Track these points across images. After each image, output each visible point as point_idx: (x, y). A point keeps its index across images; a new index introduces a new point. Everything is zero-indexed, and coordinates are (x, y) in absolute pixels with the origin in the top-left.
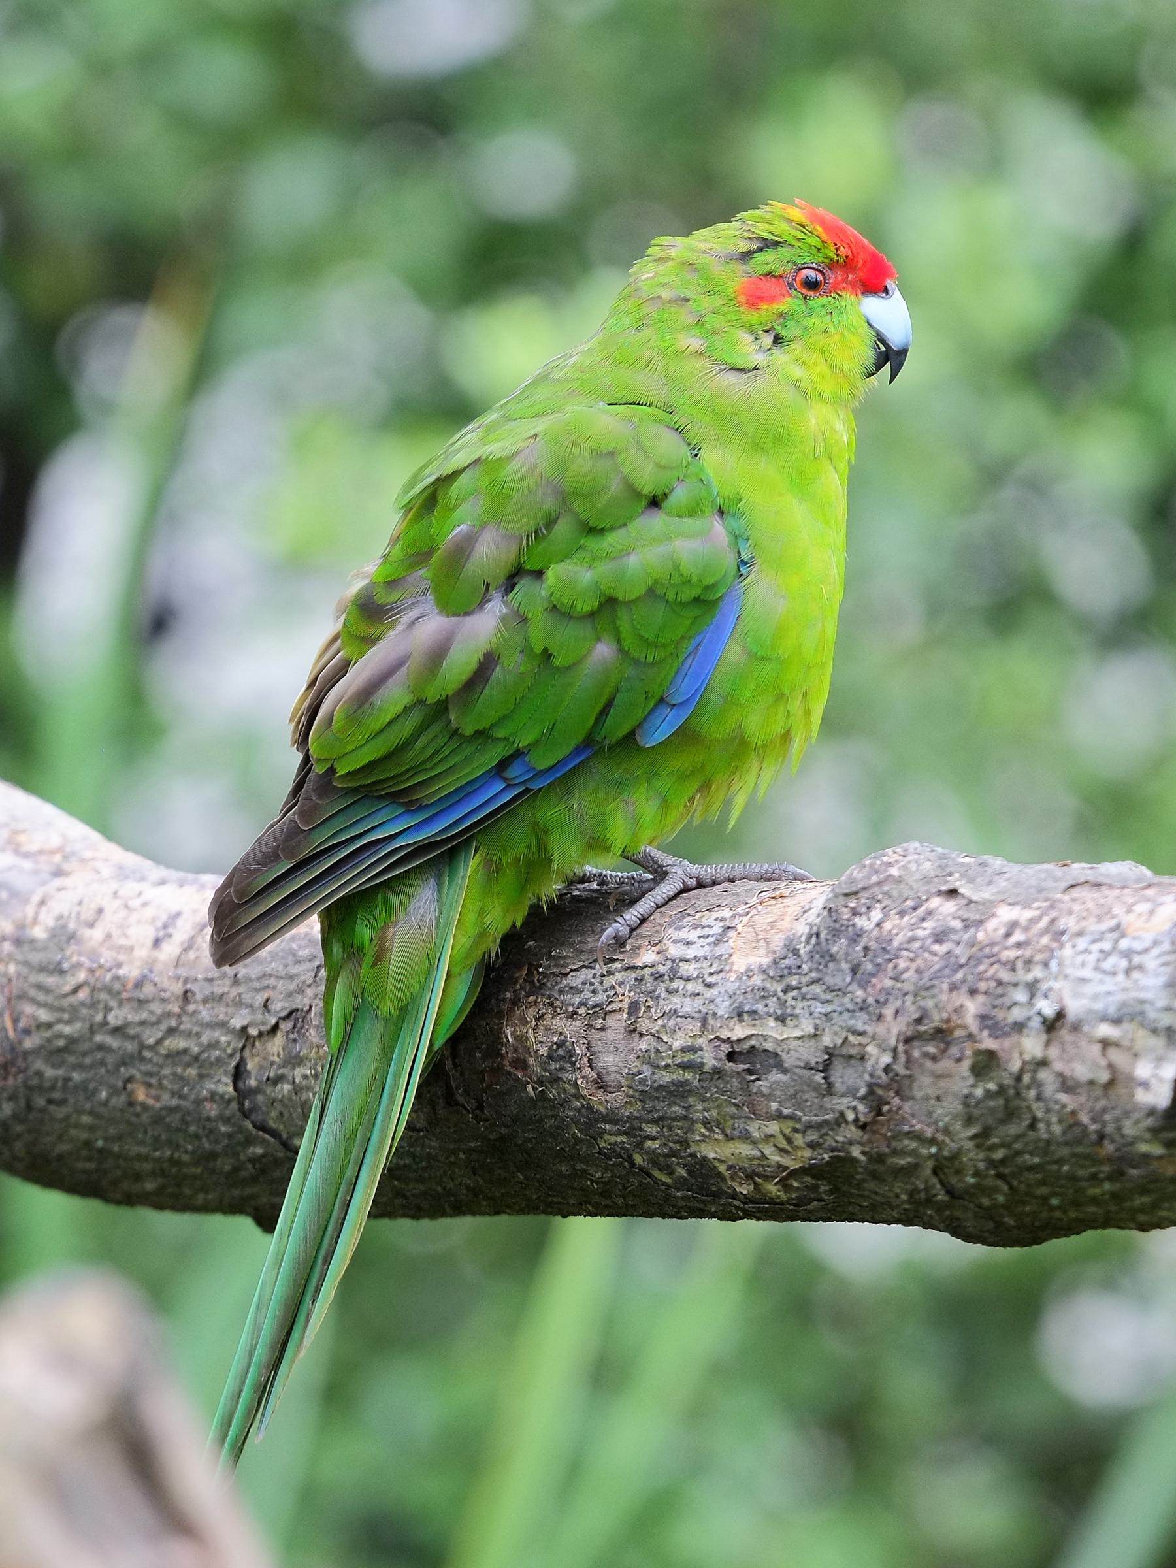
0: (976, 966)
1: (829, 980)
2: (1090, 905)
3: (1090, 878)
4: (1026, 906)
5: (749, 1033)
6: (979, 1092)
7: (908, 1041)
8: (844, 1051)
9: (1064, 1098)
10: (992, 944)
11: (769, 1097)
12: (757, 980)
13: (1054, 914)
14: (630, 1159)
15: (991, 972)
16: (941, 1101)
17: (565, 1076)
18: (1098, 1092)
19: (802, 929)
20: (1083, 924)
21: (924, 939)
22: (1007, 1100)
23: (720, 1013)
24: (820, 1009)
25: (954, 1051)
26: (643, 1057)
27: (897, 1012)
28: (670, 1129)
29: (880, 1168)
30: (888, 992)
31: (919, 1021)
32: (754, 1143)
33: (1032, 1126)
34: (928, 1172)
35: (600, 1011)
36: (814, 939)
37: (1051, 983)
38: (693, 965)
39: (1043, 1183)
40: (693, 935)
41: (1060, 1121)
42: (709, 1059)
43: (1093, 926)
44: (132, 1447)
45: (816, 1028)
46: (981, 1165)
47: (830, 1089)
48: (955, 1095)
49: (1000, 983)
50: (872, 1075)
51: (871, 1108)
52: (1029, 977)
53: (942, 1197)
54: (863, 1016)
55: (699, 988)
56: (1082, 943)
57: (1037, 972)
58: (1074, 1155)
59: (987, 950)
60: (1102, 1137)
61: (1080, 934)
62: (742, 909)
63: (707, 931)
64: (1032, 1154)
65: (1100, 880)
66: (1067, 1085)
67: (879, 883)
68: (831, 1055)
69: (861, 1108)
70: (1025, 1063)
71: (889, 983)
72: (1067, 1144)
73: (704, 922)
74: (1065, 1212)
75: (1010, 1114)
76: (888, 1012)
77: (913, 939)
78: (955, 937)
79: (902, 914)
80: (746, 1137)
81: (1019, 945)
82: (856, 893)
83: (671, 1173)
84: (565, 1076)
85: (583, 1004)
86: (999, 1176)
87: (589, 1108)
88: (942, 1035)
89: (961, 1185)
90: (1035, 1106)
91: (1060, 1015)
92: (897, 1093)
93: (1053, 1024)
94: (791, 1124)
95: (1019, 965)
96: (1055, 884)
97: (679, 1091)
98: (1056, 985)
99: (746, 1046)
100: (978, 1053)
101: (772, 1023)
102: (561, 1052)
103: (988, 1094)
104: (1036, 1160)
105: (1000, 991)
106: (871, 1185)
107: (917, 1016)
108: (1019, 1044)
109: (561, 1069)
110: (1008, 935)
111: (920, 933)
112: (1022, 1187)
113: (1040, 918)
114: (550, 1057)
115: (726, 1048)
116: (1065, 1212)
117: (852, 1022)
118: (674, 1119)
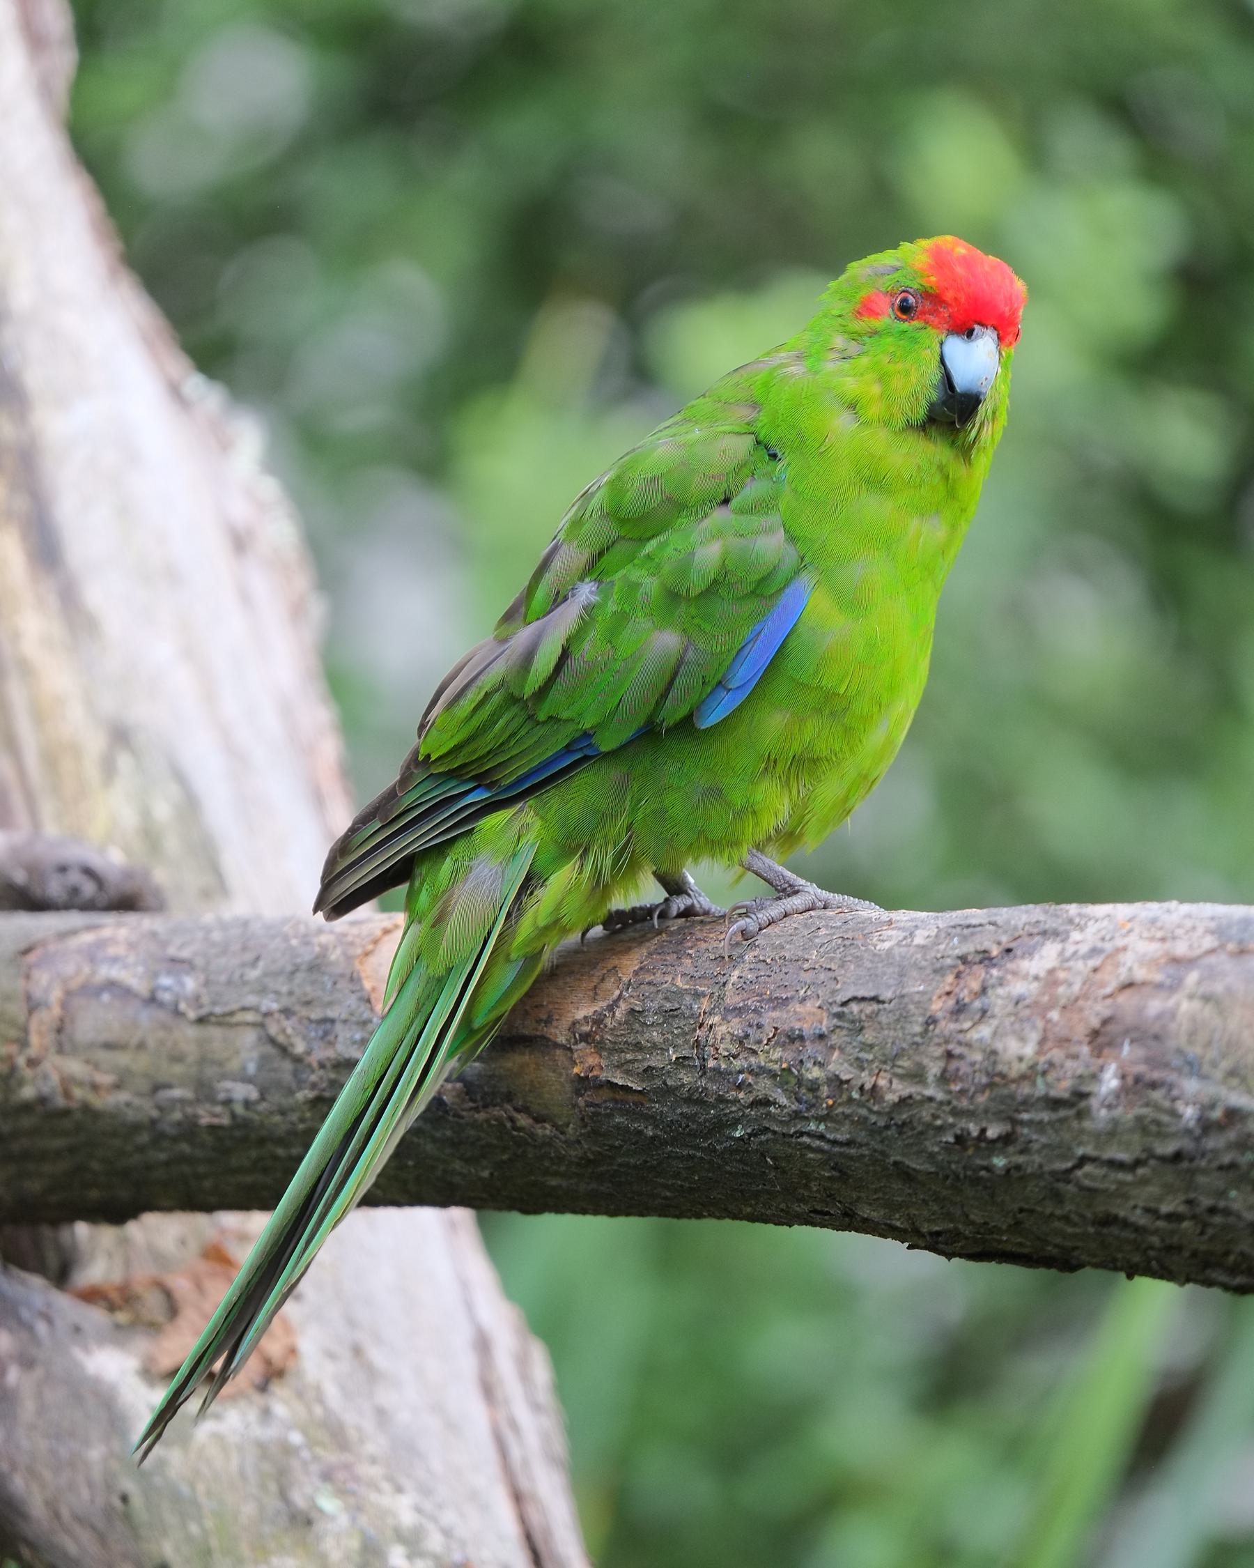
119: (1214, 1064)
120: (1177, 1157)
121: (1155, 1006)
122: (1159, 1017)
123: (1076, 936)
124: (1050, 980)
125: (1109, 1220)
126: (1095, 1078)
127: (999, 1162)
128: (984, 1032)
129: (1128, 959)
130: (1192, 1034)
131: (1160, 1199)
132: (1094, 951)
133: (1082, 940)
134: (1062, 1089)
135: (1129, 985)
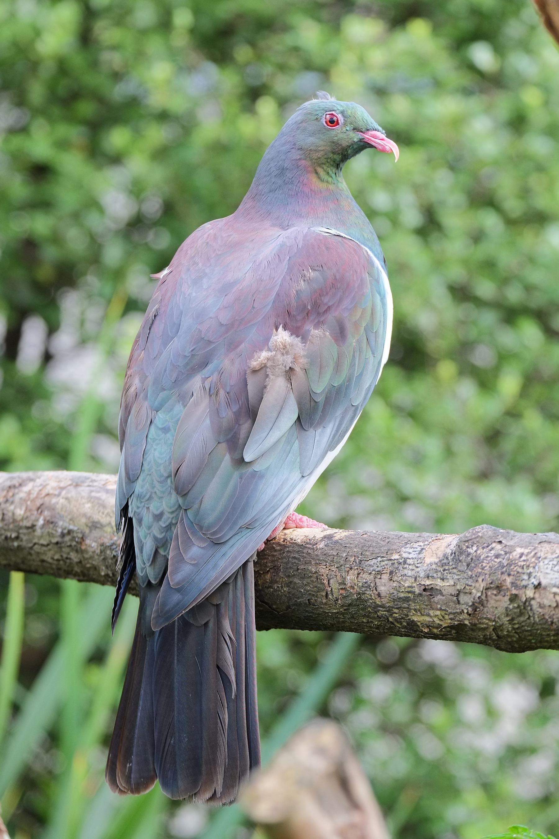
0: (510, 567)
1: (459, 568)
2: (548, 549)
3: (547, 540)
4: (526, 547)
5: (431, 583)
6: (511, 607)
7: (487, 589)
8: (464, 591)
9: (540, 610)
10: (515, 560)
11: (437, 603)
12: (434, 566)
13: (536, 551)
14: (388, 618)
15: (515, 569)
16: (498, 607)
17: (368, 592)
18: (552, 609)
19: (449, 551)
20: (546, 555)
21: (491, 557)
22: (520, 610)
23: (421, 576)
24: (456, 577)
25: (502, 593)
26: (395, 588)
27: (483, 580)
28: (402, 611)
29: (474, 628)
30: (480, 573)
31: (491, 583)
32: (431, 617)
33: (529, 618)
34: (491, 630)
35: (380, 573)
36: (453, 555)
37: (536, 574)
38: (411, 560)
39: (531, 635)
40: (411, 551)
41: (538, 617)
42: (417, 591)
43: (550, 556)
44: (344, 783)
45: (455, 583)
46: (510, 629)
47: (459, 602)
48: (502, 607)
49: (518, 572)
50: (474, 599)
51: (473, 610)
52: (528, 571)
53: (495, 637)
54: (471, 580)
55: (414, 568)
56: (546, 561)
57: (531, 570)
58: (542, 628)
59: (514, 562)
60: (552, 623)
61: (545, 558)
62: (426, 543)
63: (415, 550)
64: (528, 627)
65: (550, 540)
66: (541, 606)
67: (475, 538)
68: (459, 592)
69: (470, 609)
70: (526, 599)
71: (480, 570)
72: (540, 624)
73: (414, 546)
74: (536, 644)
75: (521, 614)
76: (480, 580)
77: (488, 557)
78: (502, 557)
79: (483, 548)
80: (428, 615)
81: (524, 561)
82: (467, 541)
83: (401, 624)
84: (368, 592)
85: (373, 570)
86: (515, 632)
87: (375, 603)
88: (499, 588)
89: (502, 635)
90: (530, 613)
91: (539, 584)
92: (482, 605)
93: (538, 587)
94: (444, 612)
95: (525, 567)
96: (535, 542)
97: (407, 599)
98: (538, 575)
99: (430, 587)
100: (512, 595)
101: (439, 580)
102: (366, 585)
103: (514, 608)
104: (529, 629)
105: (518, 575)
106: (471, 632)
107: (490, 582)
108: (525, 592)
109: (366, 590)
110: (520, 557)
111: (490, 555)
112: (523, 636)
113: (531, 552)
114: (363, 586)
115: (423, 587)
116: (536, 644)
117: (467, 582)
118: (404, 608)
119: (67, 517)
120: (57, 543)
121: (54, 500)
122: (54, 504)
123: (38, 480)
124: (29, 493)
125: (43, 561)
126: (37, 520)
127: (16, 544)
128: (12, 507)
129: (49, 487)
130: (62, 509)
131: (54, 555)
132: (41, 485)
133: (39, 482)
134: (29, 524)
135: (48, 495)
